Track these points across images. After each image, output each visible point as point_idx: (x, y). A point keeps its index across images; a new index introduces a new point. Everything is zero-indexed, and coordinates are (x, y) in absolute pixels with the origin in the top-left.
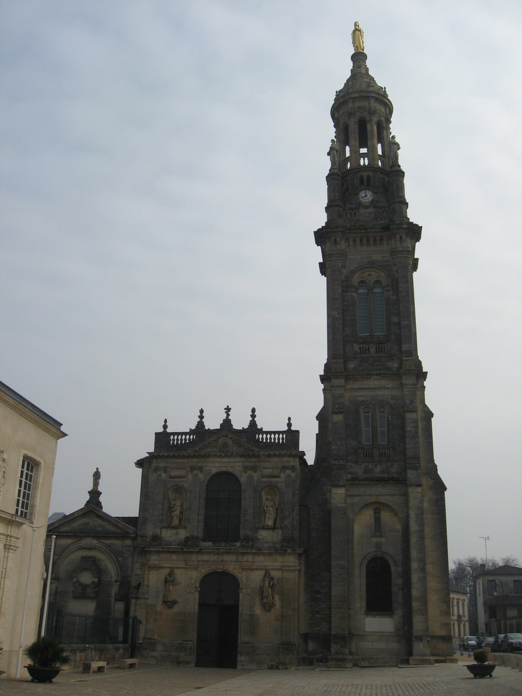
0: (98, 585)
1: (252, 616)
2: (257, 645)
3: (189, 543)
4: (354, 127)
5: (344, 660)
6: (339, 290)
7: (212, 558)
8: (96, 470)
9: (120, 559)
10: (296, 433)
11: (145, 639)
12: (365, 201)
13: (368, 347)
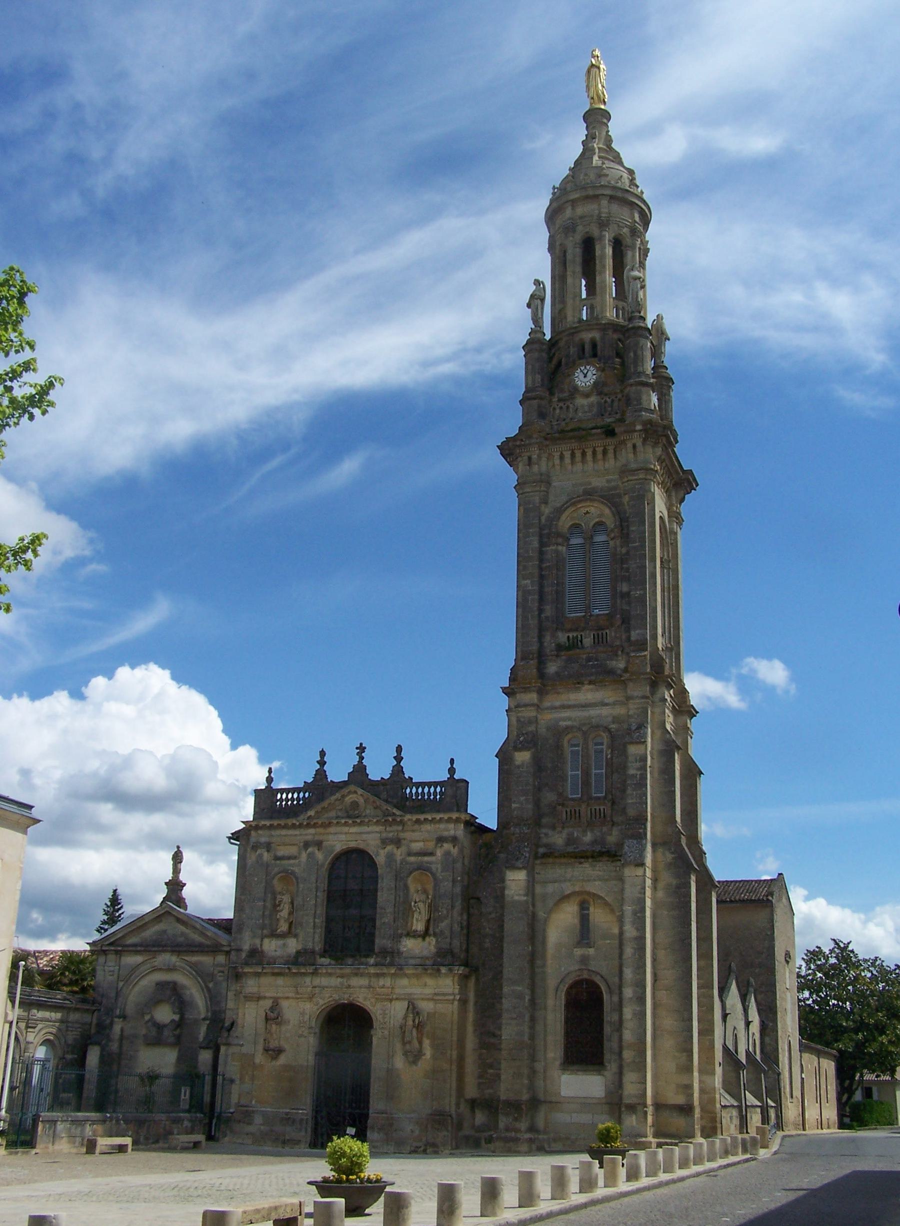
0: (179, 1025)
1: (391, 1072)
2: (396, 1116)
3: (300, 960)
4: (575, 253)
5: (516, 1140)
6: (535, 542)
7: (335, 981)
8: (176, 850)
9: (211, 985)
10: (461, 784)
11: (239, 1106)
12: (583, 384)
13: (581, 636)
